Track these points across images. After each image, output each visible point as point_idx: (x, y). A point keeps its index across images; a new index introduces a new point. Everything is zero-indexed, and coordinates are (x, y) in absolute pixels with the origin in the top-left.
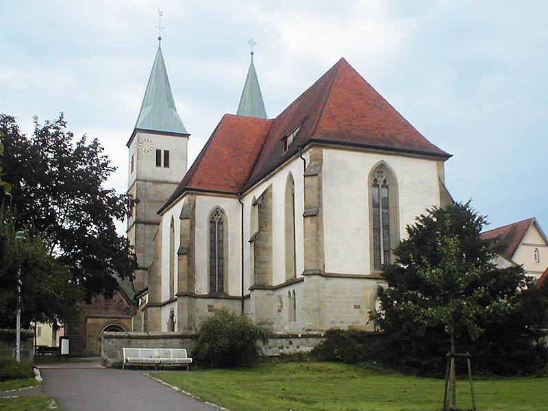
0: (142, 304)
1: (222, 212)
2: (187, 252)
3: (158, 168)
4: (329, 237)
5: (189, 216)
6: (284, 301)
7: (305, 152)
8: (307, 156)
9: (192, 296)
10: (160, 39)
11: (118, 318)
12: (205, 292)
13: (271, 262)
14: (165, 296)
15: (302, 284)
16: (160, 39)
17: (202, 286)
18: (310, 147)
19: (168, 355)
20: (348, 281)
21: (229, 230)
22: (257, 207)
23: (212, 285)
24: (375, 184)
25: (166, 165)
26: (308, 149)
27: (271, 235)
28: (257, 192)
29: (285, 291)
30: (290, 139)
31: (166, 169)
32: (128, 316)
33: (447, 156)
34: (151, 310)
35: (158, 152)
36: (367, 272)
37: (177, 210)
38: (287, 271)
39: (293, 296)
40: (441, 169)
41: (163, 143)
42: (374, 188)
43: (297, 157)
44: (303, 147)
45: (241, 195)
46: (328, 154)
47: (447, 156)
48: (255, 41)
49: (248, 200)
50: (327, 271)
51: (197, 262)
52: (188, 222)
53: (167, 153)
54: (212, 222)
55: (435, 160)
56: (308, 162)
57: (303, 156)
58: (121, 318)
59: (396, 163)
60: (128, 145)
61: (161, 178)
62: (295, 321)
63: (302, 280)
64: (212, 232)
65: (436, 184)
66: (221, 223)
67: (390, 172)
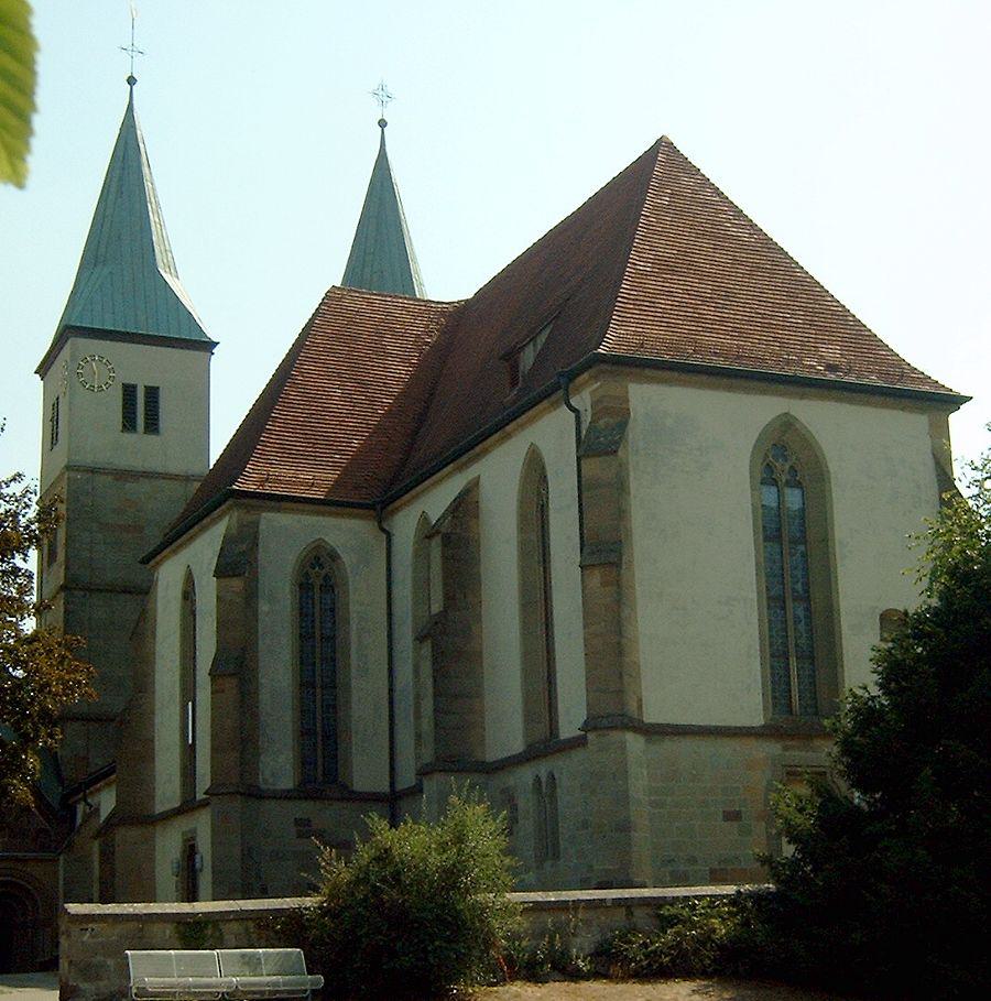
0: (84, 822)
1: (334, 556)
2: (237, 666)
3: (129, 437)
4: (650, 623)
5: (236, 564)
6: (521, 803)
7: (578, 390)
8: (583, 400)
9: (254, 793)
10: (131, 81)
11: (17, 860)
12: (287, 782)
13: (479, 695)
14: (167, 789)
15: (578, 755)
16: (131, 81)
17: (279, 765)
18: (596, 378)
19: (231, 906)
20: (705, 747)
21: (352, 608)
22: (437, 541)
23: (305, 762)
24: (767, 475)
25: (152, 425)
26: (586, 383)
27: (478, 619)
28: (436, 500)
29: (525, 776)
30: (528, 358)
31: (152, 438)
32: (47, 855)
33: (954, 401)
34: (125, 836)
35: (129, 391)
36: (758, 720)
37: (204, 550)
38: (529, 717)
39: (546, 790)
40: (941, 432)
41: (141, 365)
42: (765, 489)
43: (555, 406)
44: (572, 376)
45: (382, 509)
46: (644, 398)
47: (954, 401)
48: (390, 90)
49: (406, 524)
50: (652, 716)
51: (265, 697)
52: (236, 584)
53: (152, 394)
54: (304, 587)
55: (922, 411)
56: (587, 419)
57: (573, 402)
58: (25, 861)
59: (823, 420)
60: (43, 370)
61: (137, 464)
62: (556, 856)
63: (578, 742)
64: (304, 613)
65: (928, 476)
66: (329, 586)
67: (808, 444)
